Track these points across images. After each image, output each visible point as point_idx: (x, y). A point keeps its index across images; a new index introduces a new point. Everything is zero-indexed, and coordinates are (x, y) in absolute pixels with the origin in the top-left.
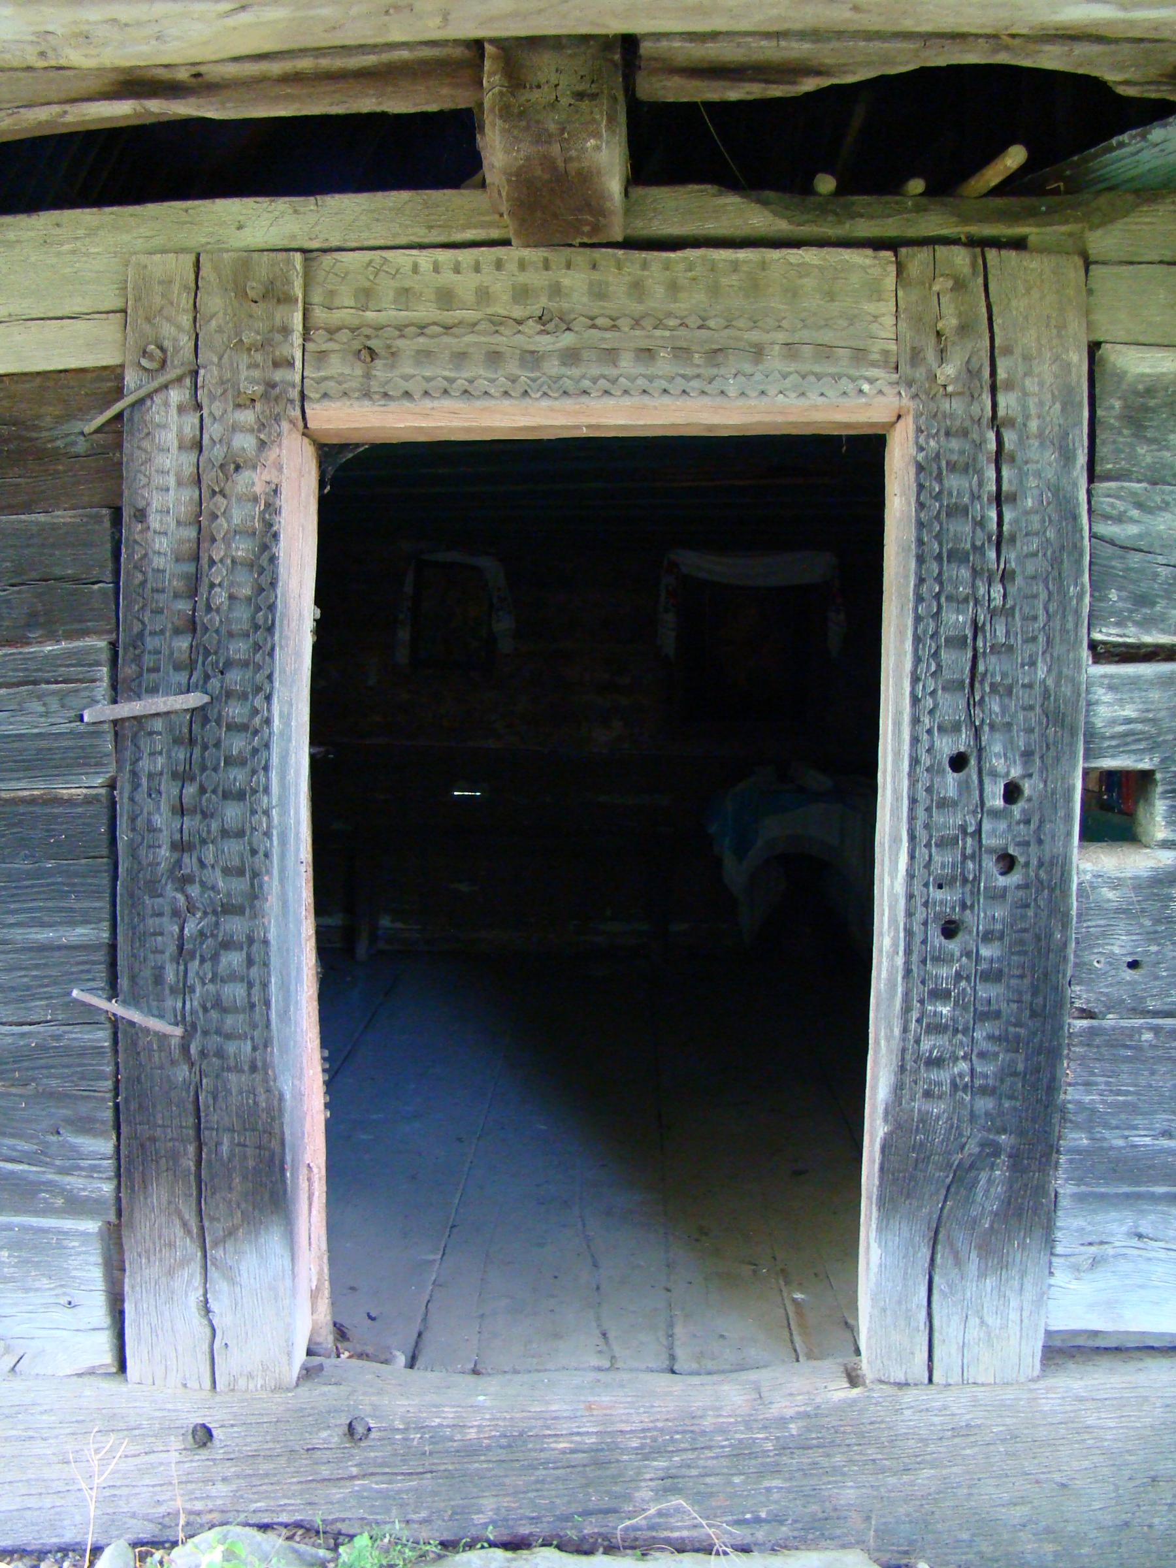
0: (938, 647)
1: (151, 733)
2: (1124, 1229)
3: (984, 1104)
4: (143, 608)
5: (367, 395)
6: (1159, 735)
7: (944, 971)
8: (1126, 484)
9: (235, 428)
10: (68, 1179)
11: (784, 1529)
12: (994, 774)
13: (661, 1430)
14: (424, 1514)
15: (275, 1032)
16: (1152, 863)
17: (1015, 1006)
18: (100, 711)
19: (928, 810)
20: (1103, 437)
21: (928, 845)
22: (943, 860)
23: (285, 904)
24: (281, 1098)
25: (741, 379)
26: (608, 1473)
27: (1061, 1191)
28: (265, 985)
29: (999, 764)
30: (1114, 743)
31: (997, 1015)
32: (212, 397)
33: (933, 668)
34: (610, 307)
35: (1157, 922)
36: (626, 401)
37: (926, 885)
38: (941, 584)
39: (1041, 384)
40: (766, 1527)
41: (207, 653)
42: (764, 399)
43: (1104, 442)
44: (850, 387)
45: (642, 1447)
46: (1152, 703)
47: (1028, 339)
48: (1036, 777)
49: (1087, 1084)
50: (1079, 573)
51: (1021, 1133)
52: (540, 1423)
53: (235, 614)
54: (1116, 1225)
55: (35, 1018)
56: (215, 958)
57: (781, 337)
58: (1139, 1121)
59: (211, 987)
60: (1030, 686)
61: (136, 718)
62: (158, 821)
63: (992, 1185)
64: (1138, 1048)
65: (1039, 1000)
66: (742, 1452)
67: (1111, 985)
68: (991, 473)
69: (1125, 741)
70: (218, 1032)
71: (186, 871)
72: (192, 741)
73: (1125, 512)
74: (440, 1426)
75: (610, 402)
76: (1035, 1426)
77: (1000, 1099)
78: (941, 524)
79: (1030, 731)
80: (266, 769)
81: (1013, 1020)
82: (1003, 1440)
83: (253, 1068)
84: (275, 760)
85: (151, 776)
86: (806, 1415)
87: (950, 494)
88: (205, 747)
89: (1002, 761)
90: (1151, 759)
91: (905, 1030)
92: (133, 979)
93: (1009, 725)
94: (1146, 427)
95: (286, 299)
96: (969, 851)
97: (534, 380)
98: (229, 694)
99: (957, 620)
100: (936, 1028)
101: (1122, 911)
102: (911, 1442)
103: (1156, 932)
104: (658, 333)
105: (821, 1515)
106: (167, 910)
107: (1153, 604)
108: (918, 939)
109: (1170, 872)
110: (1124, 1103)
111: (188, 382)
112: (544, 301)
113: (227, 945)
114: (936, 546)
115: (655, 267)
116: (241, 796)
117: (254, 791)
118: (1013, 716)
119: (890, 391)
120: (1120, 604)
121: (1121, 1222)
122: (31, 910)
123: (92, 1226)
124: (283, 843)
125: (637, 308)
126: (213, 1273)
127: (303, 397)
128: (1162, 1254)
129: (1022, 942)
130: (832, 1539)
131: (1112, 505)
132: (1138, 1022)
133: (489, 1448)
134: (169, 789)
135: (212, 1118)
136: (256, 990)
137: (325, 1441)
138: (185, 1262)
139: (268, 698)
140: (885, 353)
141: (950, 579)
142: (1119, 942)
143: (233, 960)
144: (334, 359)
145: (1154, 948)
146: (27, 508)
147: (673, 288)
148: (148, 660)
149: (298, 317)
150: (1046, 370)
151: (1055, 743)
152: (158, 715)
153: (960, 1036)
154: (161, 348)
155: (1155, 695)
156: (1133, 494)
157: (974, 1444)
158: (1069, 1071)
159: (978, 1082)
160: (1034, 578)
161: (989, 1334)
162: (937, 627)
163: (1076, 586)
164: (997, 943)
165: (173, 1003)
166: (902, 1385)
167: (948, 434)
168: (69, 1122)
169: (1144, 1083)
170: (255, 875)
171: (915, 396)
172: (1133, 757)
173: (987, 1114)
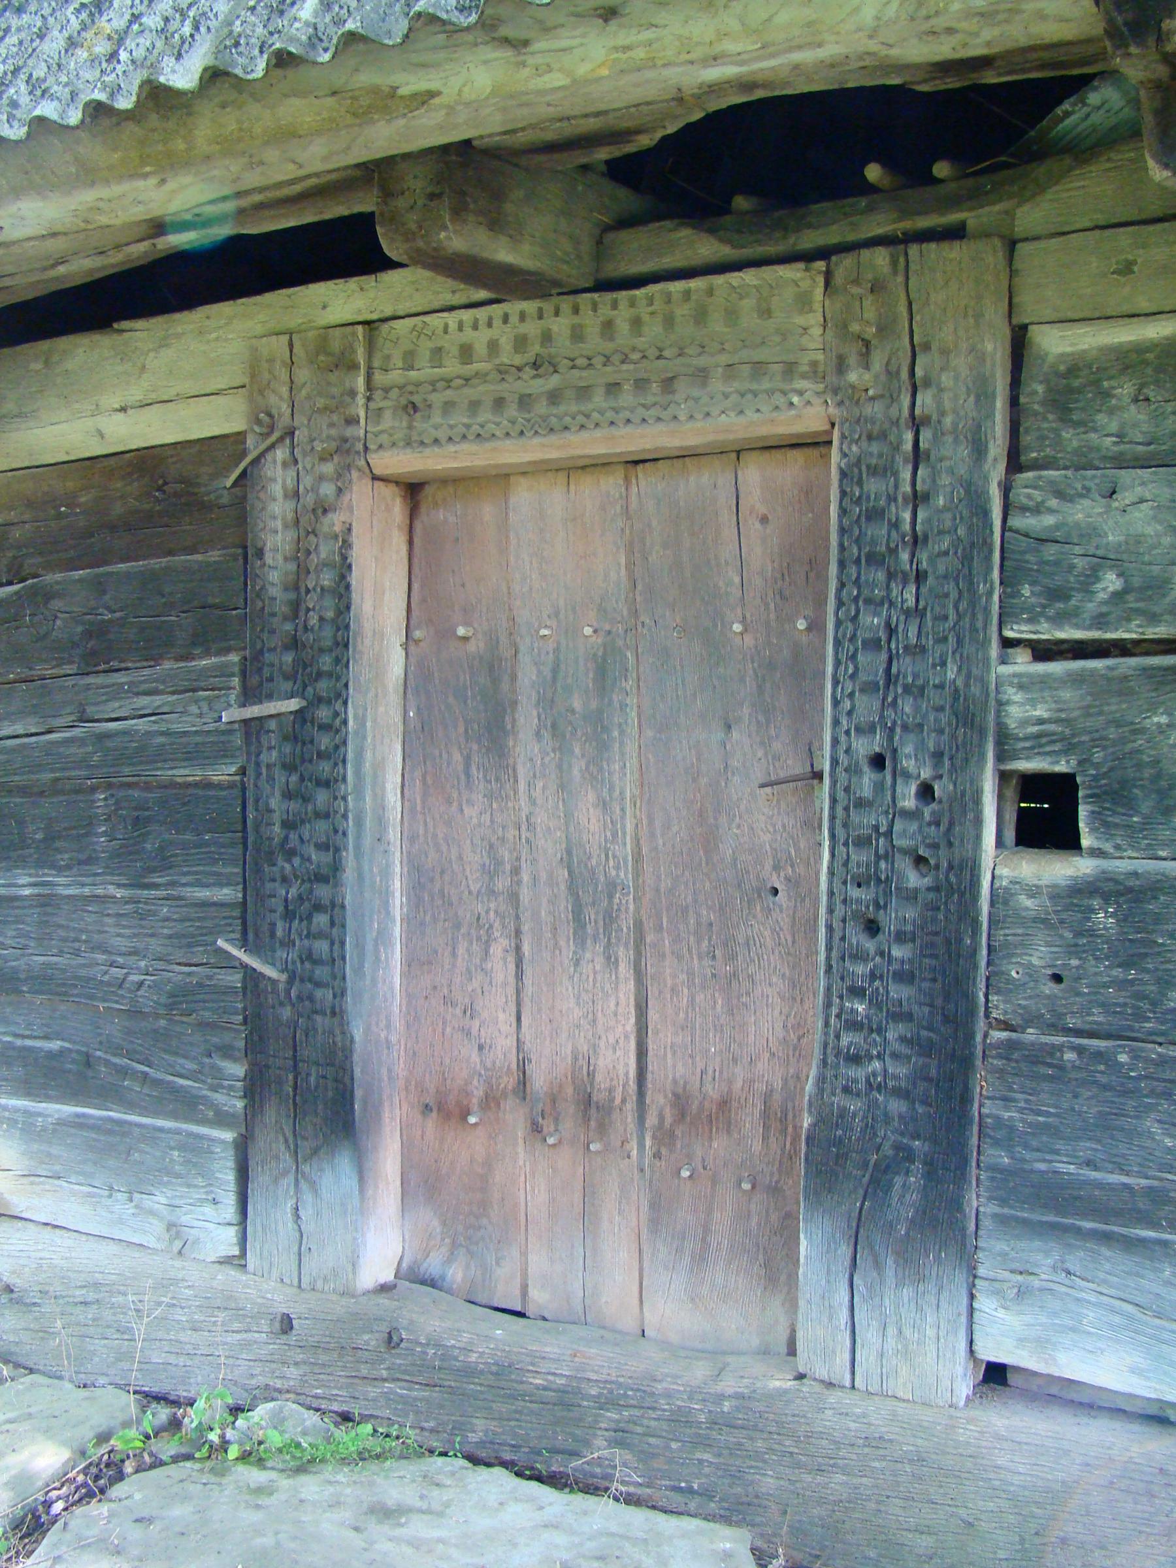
0: (856, 650)
1: (269, 731)
2: (1049, 1261)
3: (896, 1106)
4: (262, 630)
5: (408, 444)
6: (1074, 736)
7: (860, 969)
8: (1045, 473)
9: (321, 478)
10: (217, 1096)
11: (713, 1505)
12: (907, 775)
13: (620, 1385)
14: (432, 1424)
15: (349, 984)
16: (1070, 872)
17: (926, 1009)
18: (232, 714)
19: (846, 809)
20: (1027, 424)
21: (846, 844)
22: (860, 857)
23: (360, 877)
24: (352, 1041)
25: (690, 403)
26: (571, 1414)
27: (982, 1209)
28: (343, 943)
29: (909, 764)
30: (1027, 744)
31: (909, 1017)
32: (305, 455)
33: (850, 671)
34: (587, 347)
35: (1078, 934)
36: (598, 433)
37: (845, 883)
38: (859, 588)
39: (956, 378)
40: (698, 1499)
41: (305, 667)
42: (710, 420)
43: (1027, 431)
44: (780, 400)
45: (600, 1395)
46: (1065, 702)
47: (946, 335)
48: (945, 778)
49: (1005, 1099)
50: (989, 569)
51: (935, 1141)
52: (528, 1359)
53: (324, 634)
54: (1044, 1257)
55: (195, 961)
56: (310, 917)
57: (724, 359)
58: (1060, 1145)
59: (306, 942)
60: (941, 686)
61: (260, 719)
62: (274, 803)
63: (907, 1191)
64: (1061, 1068)
65: (952, 1006)
66: (680, 1419)
67: (1030, 997)
68: (906, 475)
69: (1039, 742)
70: (310, 980)
71: (291, 845)
72: (295, 738)
73: (1043, 502)
74: (453, 1347)
75: (585, 434)
76: (945, 1453)
77: (913, 1103)
78: (860, 528)
79: (941, 732)
80: (344, 761)
81: (924, 1023)
82: (911, 1461)
83: (334, 1014)
84: (350, 756)
85: (268, 766)
86: (742, 1397)
87: (868, 498)
88: (304, 743)
89: (913, 762)
90: (1068, 762)
91: (827, 1024)
92: (256, 935)
93: (920, 726)
94: (1070, 410)
95: (354, 367)
96: (881, 852)
97: (529, 421)
98: (320, 700)
99: (872, 621)
100: (854, 1025)
101: (1042, 921)
102: (824, 1442)
103: (1076, 945)
104: (625, 367)
105: (745, 1499)
106: (278, 876)
107: (1068, 598)
108: (837, 935)
109: (1088, 883)
110: (1046, 1124)
111: (288, 441)
112: (537, 348)
113: (318, 907)
114: (855, 551)
115: (623, 305)
116: (327, 784)
117: (336, 781)
118: (924, 717)
119: (817, 401)
120: (1033, 600)
121: (1047, 1254)
122: (196, 873)
123: (228, 1136)
124: (359, 823)
125: (609, 346)
126: (304, 1185)
127: (366, 449)
128: (1092, 1298)
129: (933, 945)
130: (753, 1526)
131: (1029, 497)
132: (1059, 1040)
133: (482, 1372)
134: (280, 777)
135: (304, 1053)
136: (336, 947)
137: (367, 1343)
138: (285, 1173)
139: (345, 703)
140: (814, 364)
141: (867, 581)
142: (1038, 954)
143: (321, 920)
144: (388, 414)
145: (1074, 962)
146: (192, 550)
147: (636, 322)
148: (266, 673)
149: (361, 382)
150: (961, 363)
151: (964, 743)
152: (271, 716)
153: (874, 1035)
154: (270, 416)
155: (1066, 694)
156: (1051, 482)
157: (883, 1458)
158: (982, 1083)
159: (890, 1084)
160: (945, 577)
161: (906, 1347)
162: (856, 630)
163: (985, 583)
164: (911, 945)
165: (281, 954)
166: (830, 1385)
167: (870, 438)
168: (219, 1048)
169: (1065, 1105)
170: (337, 850)
171: (840, 403)
172: (1049, 759)
173: (901, 1117)
